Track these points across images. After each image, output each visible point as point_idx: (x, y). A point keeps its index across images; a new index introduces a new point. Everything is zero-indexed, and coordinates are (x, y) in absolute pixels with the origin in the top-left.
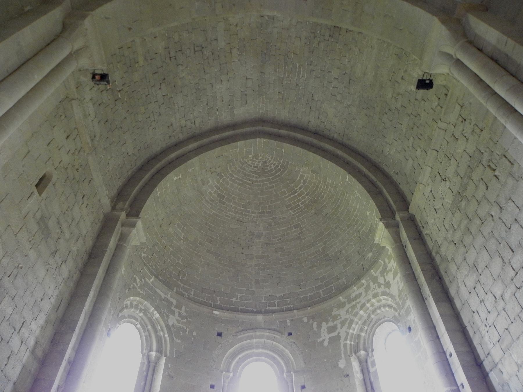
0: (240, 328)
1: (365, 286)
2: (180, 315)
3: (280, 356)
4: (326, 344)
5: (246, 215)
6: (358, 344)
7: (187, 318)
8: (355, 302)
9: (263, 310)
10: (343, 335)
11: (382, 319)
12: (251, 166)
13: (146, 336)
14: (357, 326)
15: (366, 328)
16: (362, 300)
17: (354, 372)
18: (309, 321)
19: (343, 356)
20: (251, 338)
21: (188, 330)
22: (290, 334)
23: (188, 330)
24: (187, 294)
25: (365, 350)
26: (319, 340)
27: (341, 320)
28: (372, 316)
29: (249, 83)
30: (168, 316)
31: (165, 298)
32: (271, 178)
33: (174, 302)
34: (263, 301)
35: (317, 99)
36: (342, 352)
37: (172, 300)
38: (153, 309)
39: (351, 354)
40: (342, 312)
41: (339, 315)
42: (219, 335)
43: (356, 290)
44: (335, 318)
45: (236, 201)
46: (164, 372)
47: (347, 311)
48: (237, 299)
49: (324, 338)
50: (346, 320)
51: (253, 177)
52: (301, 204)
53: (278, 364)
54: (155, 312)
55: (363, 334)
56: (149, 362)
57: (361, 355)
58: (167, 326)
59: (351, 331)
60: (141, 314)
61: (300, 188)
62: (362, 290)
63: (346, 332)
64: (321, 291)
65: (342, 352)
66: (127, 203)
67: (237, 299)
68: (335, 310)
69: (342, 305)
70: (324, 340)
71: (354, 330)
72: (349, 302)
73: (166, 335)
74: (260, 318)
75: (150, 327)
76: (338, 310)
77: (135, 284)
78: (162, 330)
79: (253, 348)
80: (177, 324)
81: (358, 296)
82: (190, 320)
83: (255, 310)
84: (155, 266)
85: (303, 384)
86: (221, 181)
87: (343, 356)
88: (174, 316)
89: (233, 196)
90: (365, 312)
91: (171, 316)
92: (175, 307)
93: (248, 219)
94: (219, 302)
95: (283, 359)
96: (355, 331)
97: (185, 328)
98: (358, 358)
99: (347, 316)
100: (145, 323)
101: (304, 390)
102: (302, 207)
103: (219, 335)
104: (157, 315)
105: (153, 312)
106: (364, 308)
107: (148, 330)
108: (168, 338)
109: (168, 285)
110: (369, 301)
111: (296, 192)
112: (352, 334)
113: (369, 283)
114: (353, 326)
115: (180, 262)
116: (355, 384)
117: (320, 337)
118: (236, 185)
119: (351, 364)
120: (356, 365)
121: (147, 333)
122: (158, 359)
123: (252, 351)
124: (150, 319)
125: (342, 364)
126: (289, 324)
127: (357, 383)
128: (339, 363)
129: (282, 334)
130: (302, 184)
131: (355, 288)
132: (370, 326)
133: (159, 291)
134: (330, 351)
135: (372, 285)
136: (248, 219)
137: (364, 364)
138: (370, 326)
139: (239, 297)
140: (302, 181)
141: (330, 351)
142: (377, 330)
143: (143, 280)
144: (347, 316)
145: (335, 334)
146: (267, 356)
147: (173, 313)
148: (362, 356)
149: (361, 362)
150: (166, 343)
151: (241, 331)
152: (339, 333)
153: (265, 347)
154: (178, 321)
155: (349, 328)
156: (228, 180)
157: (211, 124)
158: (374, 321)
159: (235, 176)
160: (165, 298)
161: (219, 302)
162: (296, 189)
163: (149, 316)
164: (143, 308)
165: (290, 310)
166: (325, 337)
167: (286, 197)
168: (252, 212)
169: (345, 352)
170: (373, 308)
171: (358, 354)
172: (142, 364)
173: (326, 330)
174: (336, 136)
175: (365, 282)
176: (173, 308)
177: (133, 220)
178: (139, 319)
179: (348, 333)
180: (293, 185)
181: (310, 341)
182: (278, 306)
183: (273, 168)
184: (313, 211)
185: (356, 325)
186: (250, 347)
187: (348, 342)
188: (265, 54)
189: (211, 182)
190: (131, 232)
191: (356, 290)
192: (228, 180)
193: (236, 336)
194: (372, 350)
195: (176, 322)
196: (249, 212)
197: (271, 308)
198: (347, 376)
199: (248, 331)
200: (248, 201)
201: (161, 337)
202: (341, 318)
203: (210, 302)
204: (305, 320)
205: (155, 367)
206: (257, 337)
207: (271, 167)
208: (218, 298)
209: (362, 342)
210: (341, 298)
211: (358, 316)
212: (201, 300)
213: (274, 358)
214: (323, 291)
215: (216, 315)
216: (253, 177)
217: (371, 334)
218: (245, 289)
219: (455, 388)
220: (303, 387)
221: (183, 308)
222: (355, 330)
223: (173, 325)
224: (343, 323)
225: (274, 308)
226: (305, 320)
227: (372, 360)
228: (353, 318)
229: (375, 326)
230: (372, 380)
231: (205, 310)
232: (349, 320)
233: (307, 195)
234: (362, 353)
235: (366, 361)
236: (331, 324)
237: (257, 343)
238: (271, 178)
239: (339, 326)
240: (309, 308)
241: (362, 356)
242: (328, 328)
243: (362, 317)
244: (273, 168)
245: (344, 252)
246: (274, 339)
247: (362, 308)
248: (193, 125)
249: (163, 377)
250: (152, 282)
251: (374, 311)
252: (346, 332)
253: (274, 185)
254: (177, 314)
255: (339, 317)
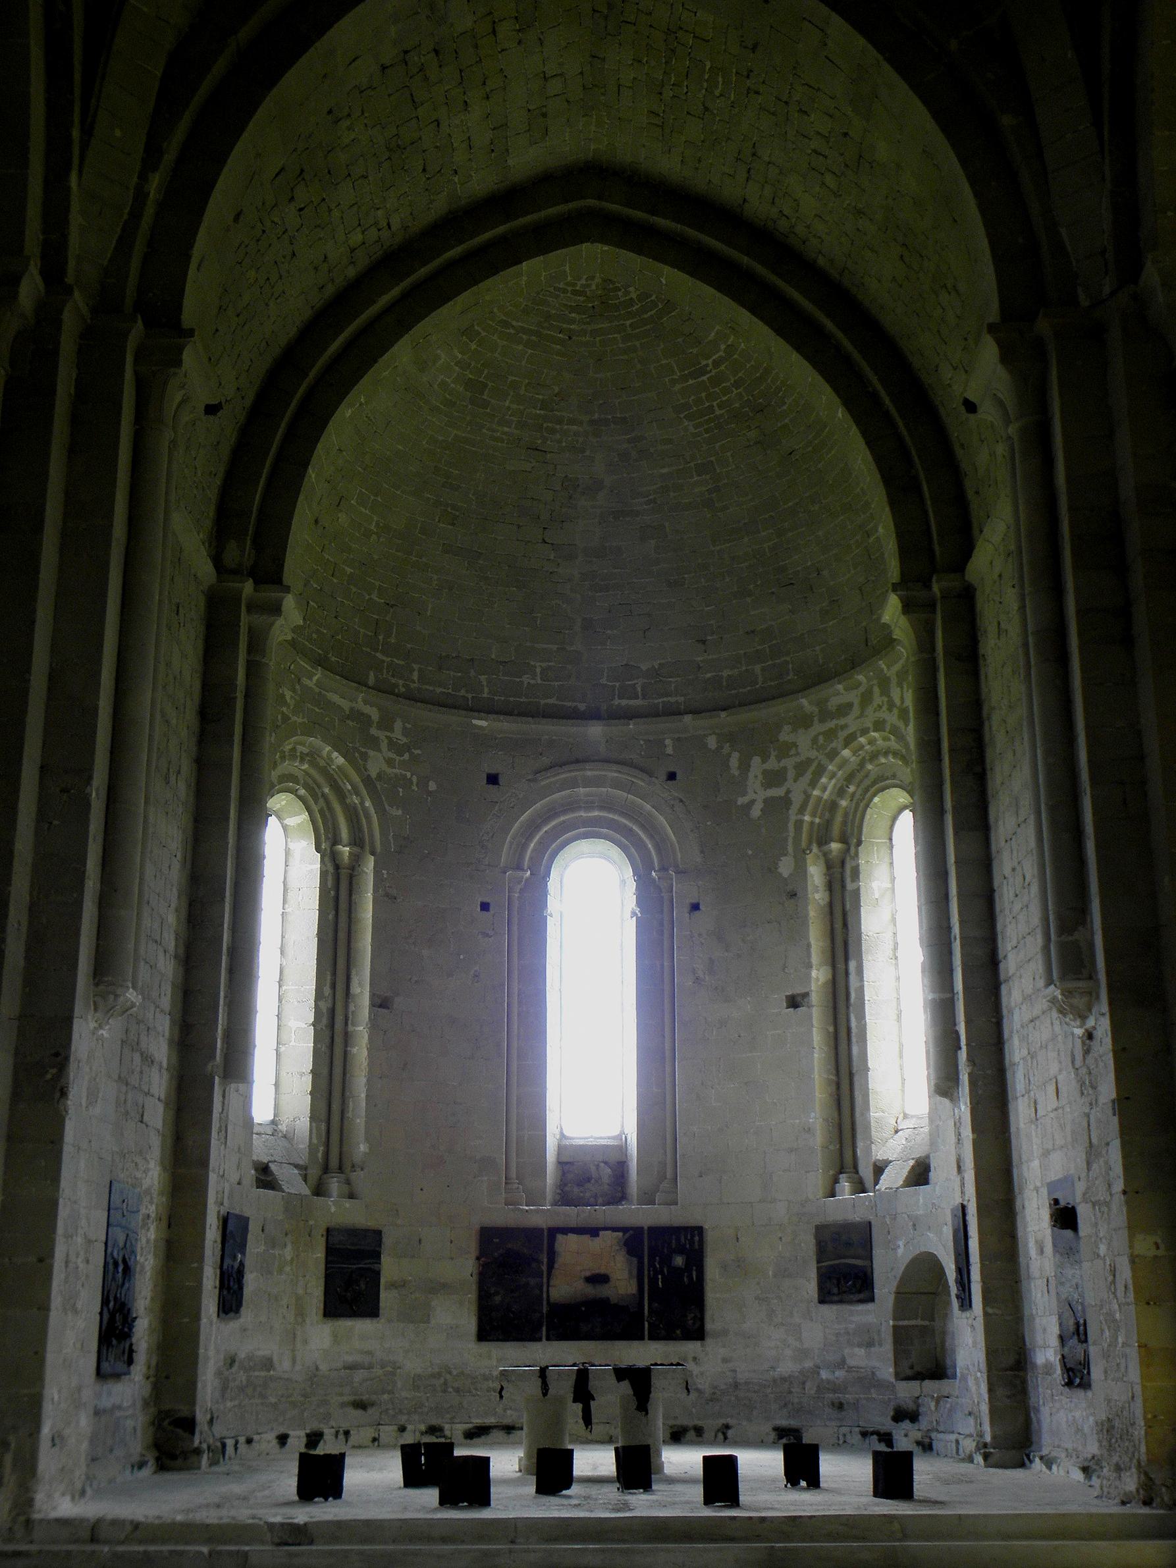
0: (546, 760)
1: (862, 689)
2: (392, 744)
3: (642, 827)
4: (756, 812)
5: (553, 431)
6: (828, 824)
7: (409, 750)
8: (835, 722)
9: (604, 707)
10: (797, 799)
11: (888, 778)
12: (565, 291)
13: (321, 812)
14: (833, 781)
15: (852, 789)
16: (851, 722)
17: (810, 888)
18: (720, 748)
19: (790, 849)
20: (573, 784)
21: (415, 779)
22: (672, 776)
23: (415, 779)
24: (401, 682)
25: (844, 840)
26: (741, 801)
27: (798, 759)
28: (870, 767)
29: (555, 86)
30: (364, 757)
31: (352, 709)
32: (628, 323)
33: (374, 713)
34: (604, 681)
35: (767, 159)
36: (790, 840)
37: (367, 710)
38: (328, 748)
39: (809, 848)
40: (803, 739)
41: (795, 745)
42: (493, 779)
43: (842, 691)
44: (785, 750)
45: (522, 392)
46: (375, 891)
47: (815, 741)
48: (534, 677)
49: (754, 796)
50: (809, 761)
51: (573, 321)
52: (720, 407)
53: (640, 845)
54: (335, 754)
55: (844, 803)
56: (337, 867)
57: (831, 851)
58: (368, 781)
59: (816, 793)
60: (305, 767)
61: (716, 364)
62: (853, 697)
63: (805, 792)
64: (757, 668)
65: (790, 840)
66: (249, 542)
67: (534, 677)
68: (787, 728)
69: (804, 721)
70: (753, 802)
71: (824, 789)
72: (825, 715)
73: (368, 804)
74: (595, 731)
75: (327, 790)
76: (794, 730)
77: (284, 709)
78: (357, 794)
79: (579, 808)
80: (389, 771)
81: (843, 710)
82: (419, 752)
83: (582, 707)
84: (318, 632)
85: (694, 901)
86: (473, 346)
87: (790, 849)
88: (379, 750)
89: (511, 378)
90: (855, 753)
91: (371, 753)
92: (379, 728)
93: (560, 442)
94: (486, 690)
95: (651, 837)
96: (827, 793)
97: (409, 775)
98: (825, 855)
99: (813, 754)
100: (315, 781)
101: (697, 913)
102: (722, 415)
103: (493, 779)
104: (340, 760)
105: (329, 753)
106: (854, 744)
107: (323, 795)
108: (372, 811)
109: (353, 676)
110: (864, 732)
111: (703, 371)
112: (820, 799)
113: (872, 686)
114: (824, 780)
115: (374, 597)
116: (807, 916)
117: (744, 794)
118: (520, 347)
119: (806, 871)
120: (816, 873)
121: (321, 801)
122: (356, 859)
123: (576, 814)
124: (324, 772)
125: (786, 867)
126: (669, 750)
127: (812, 914)
128: (781, 864)
129: (650, 774)
130: (721, 353)
131: (840, 687)
132: (863, 786)
133: (335, 698)
134: (764, 830)
135: (878, 699)
136: (560, 442)
137: (837, 870)
138: (863, 786)
139: (538, 670)
140: (723, 347)
141: (764, 830)
142: (876, 800)
143: (298, 687)
144: (813, 754)
145: (778, 792)
146: (612, 825)
147: (374, 743)
148: (834, 854)
149: (829, 866)
150: (368, 817)
151: (546, 769)
152: (788, 792)
153: (606, 805)
154: (390, 762)
155: (813, 783)
156: (495, 337)
157: (439, 206)
158: (872, 777)
159: (514, 323)
160: (352, 709)
161: (486, 690)
162: (704, 363)
163: (322, 763)
164: (305, 750)
165: (673, 712)
166: (756, 794)
167: (674, 382)
168: (572, 422)
169: (797, 839)
170: (874, 748)
171: (825, 848)
172: (323, 874)
173: (760, 777)
174: (821, 261)
175: (865, 680)
176: (374, 731)
177: (270, 594)
178: (300, 774)
179: (808, 796)
180: (695, 351)
181: (719, 799)
182: (644, 698)
183: (634, 296)
184: (753, 434)
185: (831, 778)
186: (570, 806)
187: (807, 818)
188: (606, 18)
189: (443, 356)
190: (272, 624)
191: (842, 691)
192: (495, 337)
193: (534, 780)
194: (859, 843)
195: (385, 767)
196: (560, 421)
197: (624, 702)
198: (793, 895)
199: (566, 768)
200: (557, 389)
201: (355, 808)
202: (798, 754)
203: (463, 693)
204: (712, 742)
205: (351, 877)
206: (588, 783)
207: (627, 293)
208: (483, 678)
209: (839, 819)
210: (804, 702)
211: (837, 760)
212: (439, 690)
213: (631, 830)
214: (763, 669)
215: (481, 728)
216: (573, 321)
217: (862, 804)
218: (555, 647)
219: (948, 995)
220: (695, 907)
221: (398, 725)
222: (826, 788)
223: (380, 776)
224: (801, 768)
225: (632, 702)
226: (712, 742)
227: (854, 864)
228: (824, 761)
229: (873, 790)
230: (848, 906)
231: (454, 719)
232: (815, 764)
233: (737, 384)
234: (835, 846)
235: (843, 863)
236: (772, 764)
237: (587, 795)
238: (628, 323)
239: (791, 774)
240: (723, 714)
241: (834, 854)
242: (765, 773)
243: (845, 762)
244: (634, 296)
245: (825, 573)
246: (630, 788)
247: (848, 742)
248: (385, 234)
249: (375, 901)
250: (318, 684)
251: (874, 756)
252: (805, 792)
253: (637, 344)
254: (384, 745)
255: (793, 752)
